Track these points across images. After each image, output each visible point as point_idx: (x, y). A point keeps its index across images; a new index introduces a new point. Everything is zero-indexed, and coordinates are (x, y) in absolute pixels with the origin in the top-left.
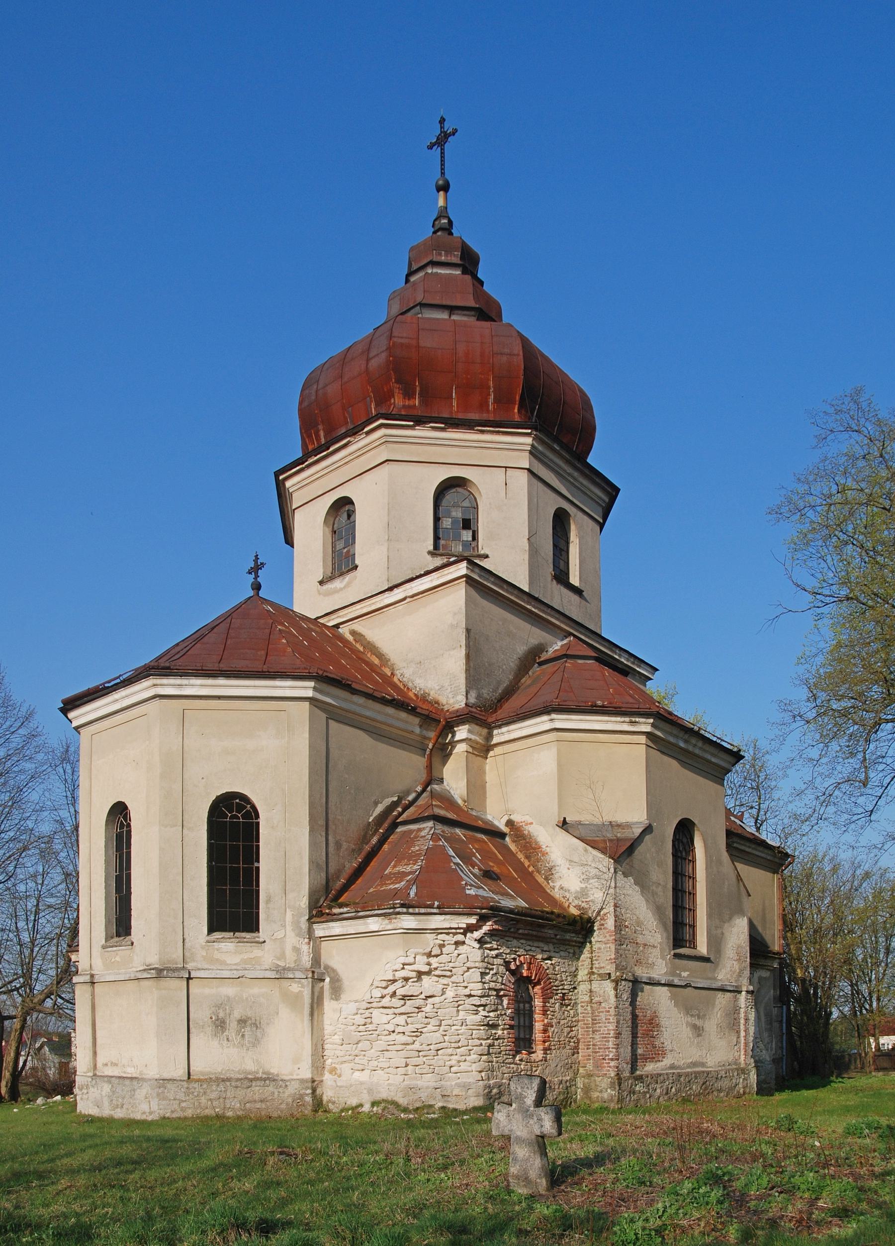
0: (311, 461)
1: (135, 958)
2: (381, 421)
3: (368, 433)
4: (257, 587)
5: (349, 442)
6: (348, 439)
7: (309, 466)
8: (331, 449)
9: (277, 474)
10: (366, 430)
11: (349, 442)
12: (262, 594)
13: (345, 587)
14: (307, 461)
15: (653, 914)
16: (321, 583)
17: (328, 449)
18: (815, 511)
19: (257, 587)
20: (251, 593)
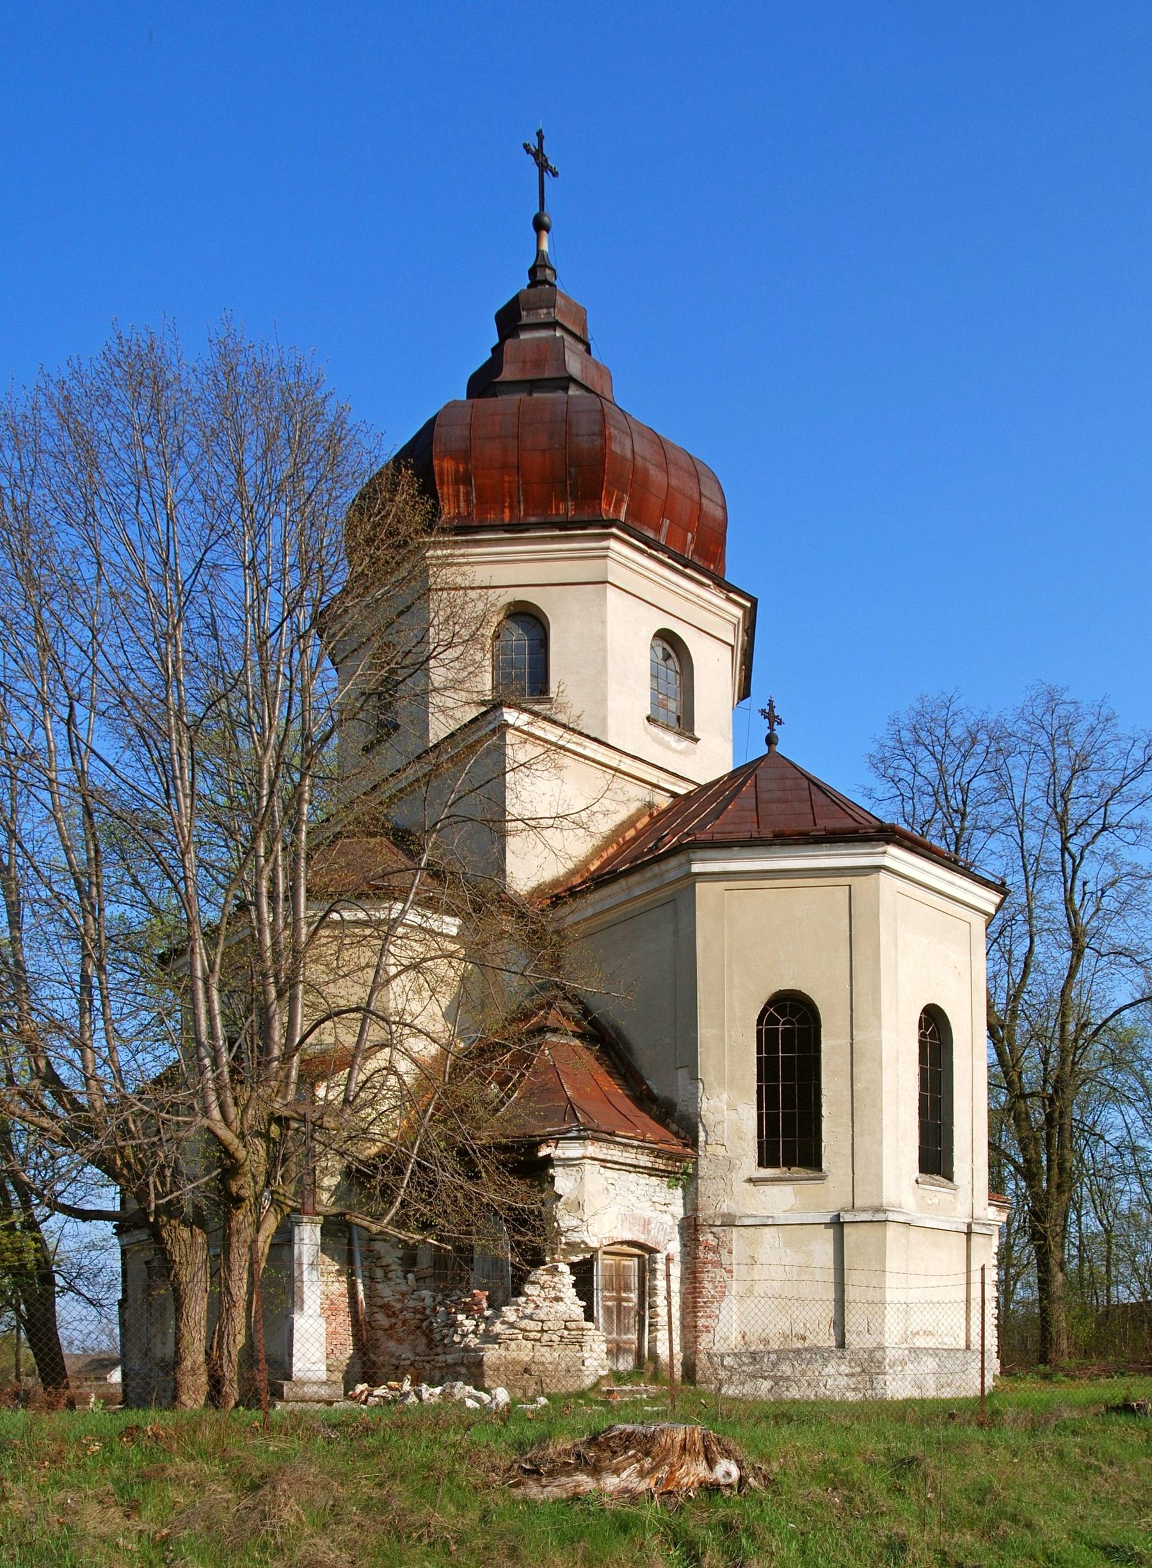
0: (660, 556)
1: (959, 1206)
2: (614, 530)
3: (729, 599)
4: (770, 740)
5: (709, 586)
6: (710, 583)
7: (651, 557)
8: (688, 571)
9: (754, 601)
10: (731, 595)
11: (709, 586)
12: (778, 749)
13: (680, 752)
14: (656, 550)
15: (301, 1288)
16: (367, 750)
17: (685, 566)
18: (167, 697)
19: (770, 740)
20: (764, 750)
